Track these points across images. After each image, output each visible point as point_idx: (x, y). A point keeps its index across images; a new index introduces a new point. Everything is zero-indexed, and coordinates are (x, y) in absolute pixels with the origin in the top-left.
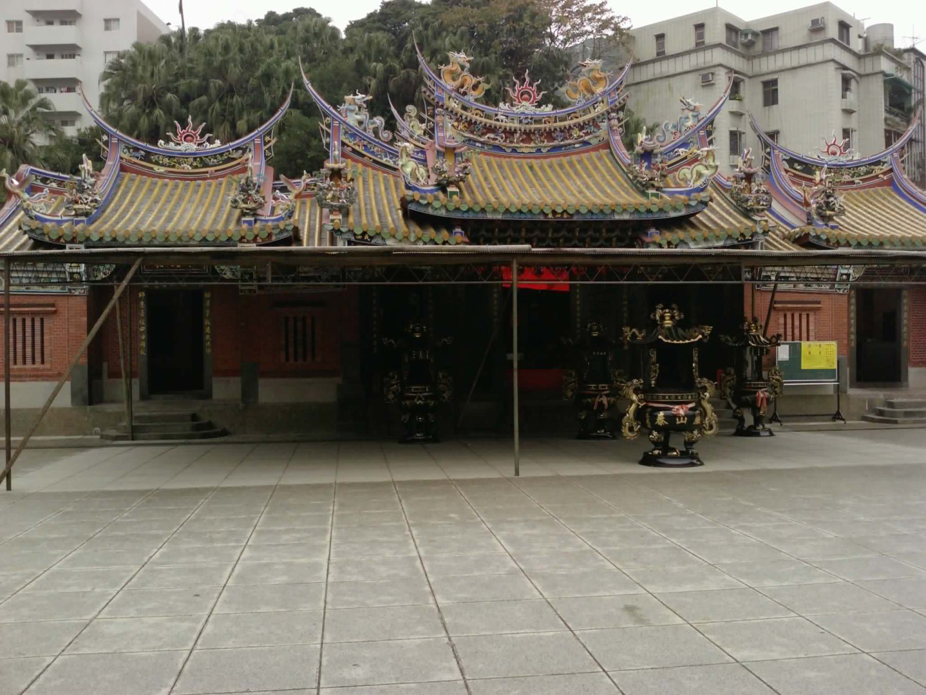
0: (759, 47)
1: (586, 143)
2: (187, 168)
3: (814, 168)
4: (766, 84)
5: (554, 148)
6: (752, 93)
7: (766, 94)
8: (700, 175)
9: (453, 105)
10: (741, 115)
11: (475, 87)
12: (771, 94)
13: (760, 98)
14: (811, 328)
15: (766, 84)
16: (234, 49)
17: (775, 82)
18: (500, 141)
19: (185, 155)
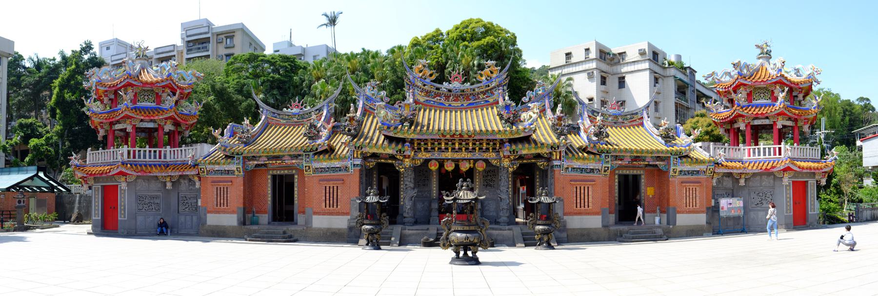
0: (616, 60)
1: (487, 101)
2: (295, 120)
3: (443, 171)
4: (620, 78)
5: (470, 104)
6: (613, 82)
7: (620, 82)
8: (531, 117)
9: (420, 84)
10: (656, 102)
11: (431, 75)
12: (622, 82)
13: (617, 84)
14: (590, 199)
15: (620, 78)
16: (569, 89)
17: (624, 78)
18: (442, 101)
19: (294, 115)
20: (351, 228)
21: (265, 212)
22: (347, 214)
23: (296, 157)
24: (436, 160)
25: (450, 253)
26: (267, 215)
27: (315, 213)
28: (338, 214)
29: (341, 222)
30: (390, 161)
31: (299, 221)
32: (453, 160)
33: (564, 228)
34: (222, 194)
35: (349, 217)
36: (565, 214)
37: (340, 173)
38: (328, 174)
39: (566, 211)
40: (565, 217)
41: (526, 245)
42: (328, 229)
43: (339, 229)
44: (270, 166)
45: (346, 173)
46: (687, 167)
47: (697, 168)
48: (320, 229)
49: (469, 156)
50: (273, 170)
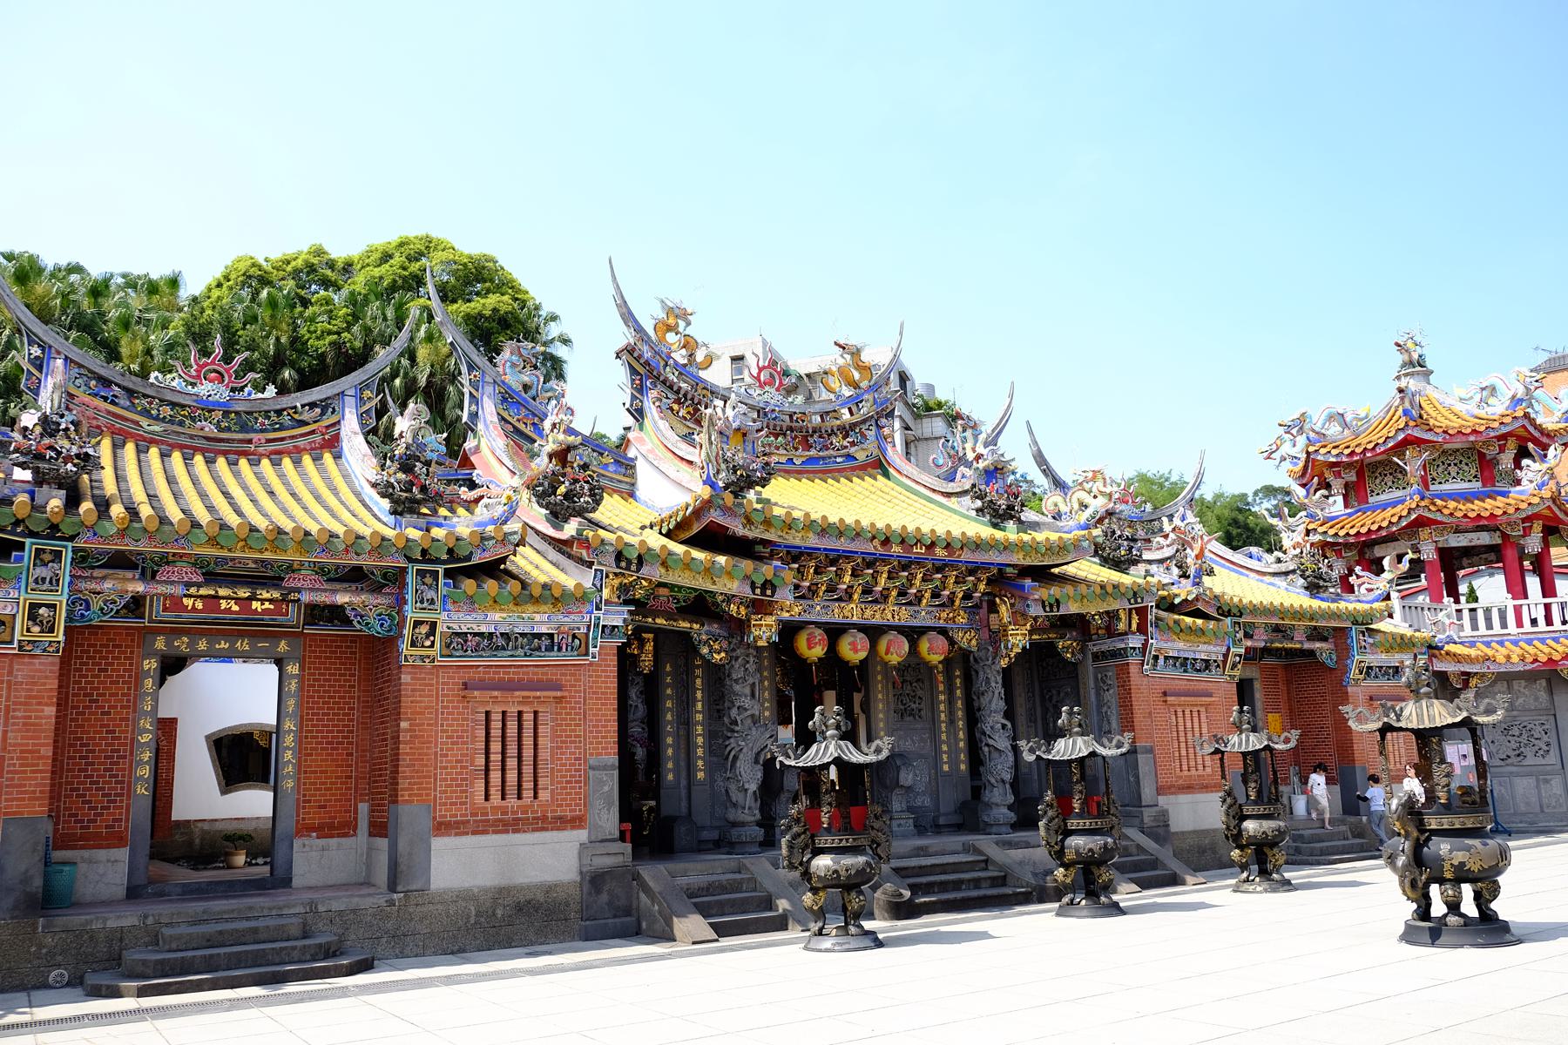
1: (849, 457)
2: (210, 429)
5: (811, 460)
19: (207, 407)
20: (595, 880)
21: (116, 840)
22: (576, 822)
23: (355, 577)
24: (818, 624)
25: (1375, 894)
26: (123, 854)
27: (444, 828)
28: (544, 823)
29: (551, 859)
30: (685, 625)
31: (297, 870)
32: (866, 629)
33: (1160, 831)
34: (509, 756)
35: (582, 835)
36: (1160, 790)
37: (553, 658)
38: (502, 659)
39: (1162, 782)
40: (1162, 800)
41: (722, 931)
42: (502, 892)
43: (549, 889)
44: (156, 612)
45: (571, 659)
46: (495, 620)
47: (541, 621)
48: (465, 896)
49: (904, 616)
50: (174, 632)
